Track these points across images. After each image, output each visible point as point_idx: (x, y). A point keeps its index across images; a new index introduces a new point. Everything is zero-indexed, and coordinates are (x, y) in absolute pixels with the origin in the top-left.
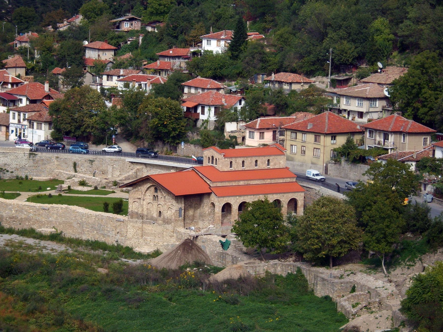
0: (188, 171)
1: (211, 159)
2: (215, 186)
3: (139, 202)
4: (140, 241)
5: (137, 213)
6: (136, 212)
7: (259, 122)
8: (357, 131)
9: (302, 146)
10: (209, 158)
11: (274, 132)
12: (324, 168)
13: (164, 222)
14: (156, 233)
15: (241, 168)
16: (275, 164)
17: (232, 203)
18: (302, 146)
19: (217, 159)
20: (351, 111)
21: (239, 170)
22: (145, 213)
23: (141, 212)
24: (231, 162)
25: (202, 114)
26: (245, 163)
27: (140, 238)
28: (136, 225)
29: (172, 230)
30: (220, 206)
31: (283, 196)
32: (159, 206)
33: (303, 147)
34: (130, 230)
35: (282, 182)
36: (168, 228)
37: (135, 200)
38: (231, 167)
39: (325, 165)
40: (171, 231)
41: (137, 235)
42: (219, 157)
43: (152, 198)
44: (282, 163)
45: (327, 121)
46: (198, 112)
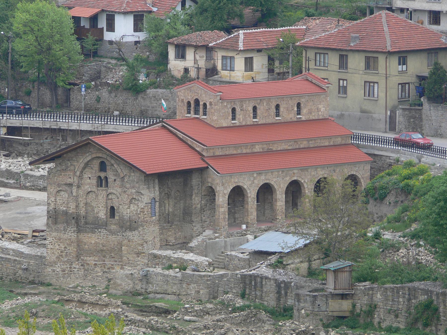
2: (212, 155)
4: (74, 265)
5: (66, 213)
6: (63, 211)
7: (242, 37)
8: (444, 46)
10: (189, 103)
11: (271, 60)
12: (388, 120)
13: (122, 227)
15: (250, 120)
16: (310, 112)
17: (245, 187)
18: (339, 80)
19: (208, 104)
20: (415, 11)
21: (249, 123)
22: (82, 212)
23: (74, 211)
24: (234, 110)
25: (108, 30)
26: (258, 112)
29: (139, 242)
30: (225, 192)
33: (341, 82)
34: (52, 247)
36: (131, 237)
37: (61, 189)
38: (234, 119)
39: (389, 113)
40: (139, 244)
41: (66, 256)
42: (212, 100)
43: (94, 182)
44: (323, 109)
45: (386, 29)
46: (100, 26)
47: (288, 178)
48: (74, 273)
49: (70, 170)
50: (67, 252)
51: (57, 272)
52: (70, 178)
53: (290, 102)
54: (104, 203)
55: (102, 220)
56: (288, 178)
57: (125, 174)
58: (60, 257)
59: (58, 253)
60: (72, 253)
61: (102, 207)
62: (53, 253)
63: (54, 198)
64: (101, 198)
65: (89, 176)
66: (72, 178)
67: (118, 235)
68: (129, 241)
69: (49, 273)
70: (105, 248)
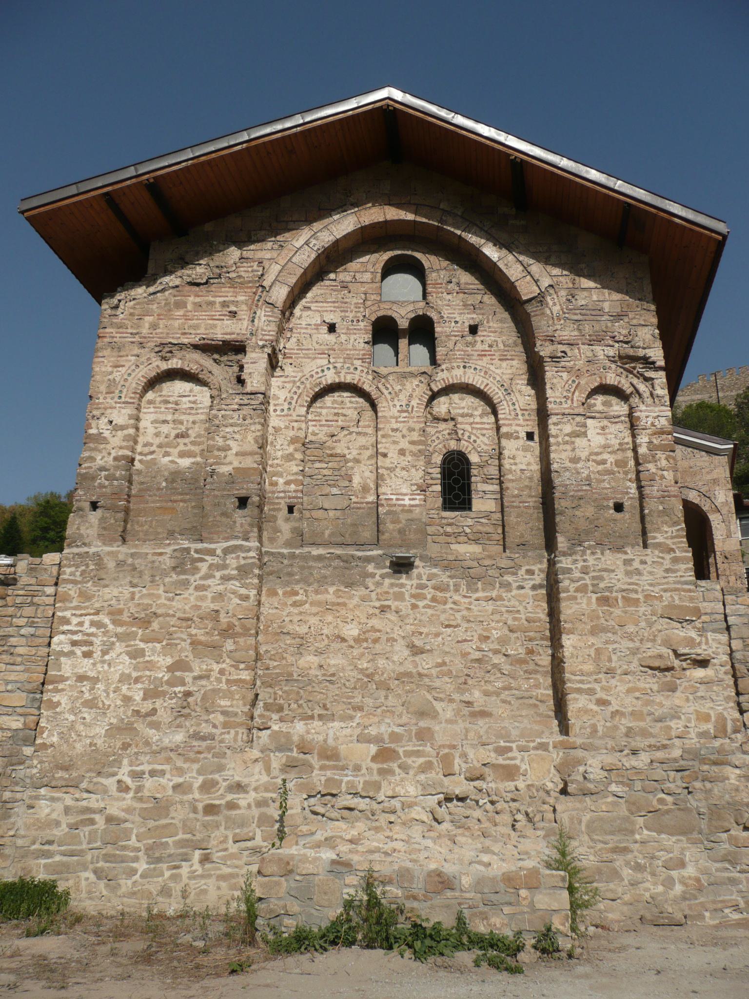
4: (234, 772)
6: (175, 476)
14: (425, 663)
27: (235, 736)
32: (442, 406)
34: (85, 666)
36: (619, 579)
41: (182, 712)
48: (231, 823)
49: (232, 283)
50: (188, 694)
51: (110, 820)
52: (233, 314)
54: (415, 436)
55: (403, 517)
57: (545, 282)
58: (140, 726)
59: (127, 699)
60: (229, 695)
61: (402, 452)
62: (91, 704)
63: (129, 411)
64: (394, 412)
65: (330, 318)
66: (244, 313)
67: (507, 586)
68: (604, 601)
69: (48, 834)
70: (425, 663)
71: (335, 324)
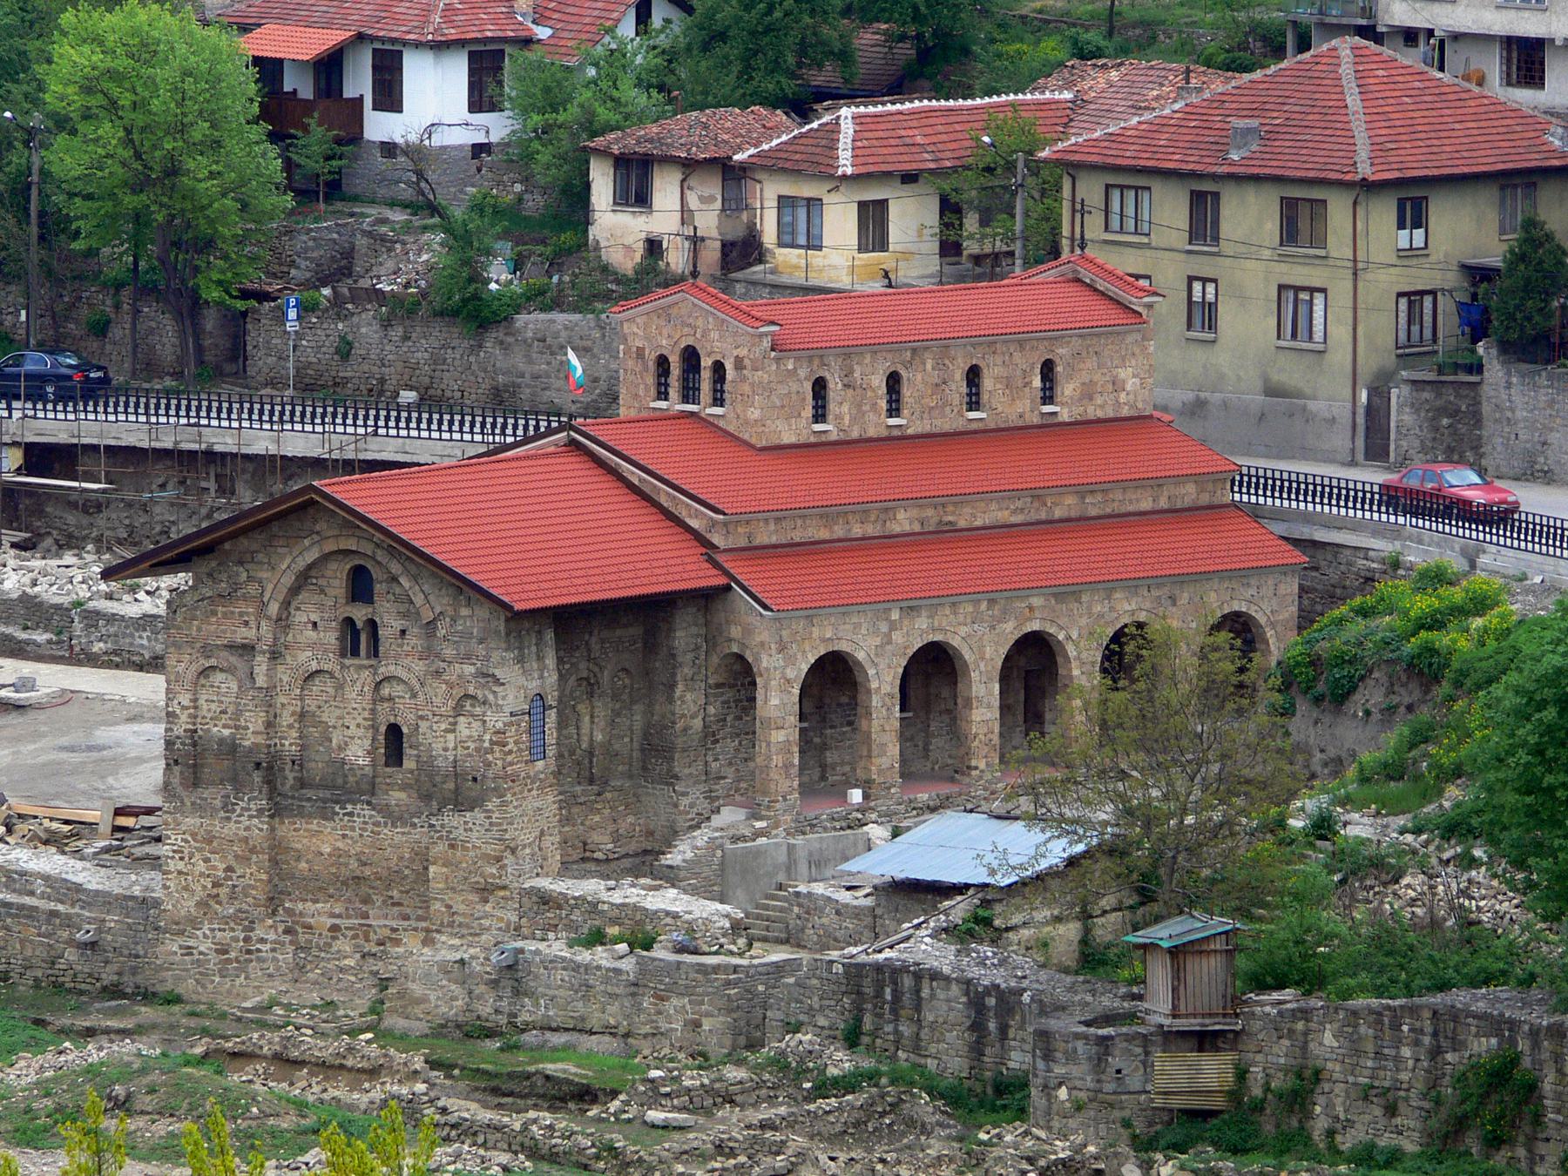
0: (536, 457)
1: (675, 371)
2: (743, 543)
3: (242, 673)
4: (259, 932)
5: (230, 748)
6: (221, 741)
7: (847, 129)
8: (1556, 163)
9: (1191, 279)
10: (662, 362)
11: (950, 209)
12: (1361, 420)
13: (426, 798)
15: (878, 423)
16: (1088, 394)
17: (860, 656)
18: (1191, 279)
19: (729, 366)
21: (872, 432)
22: (289, 744)
23: (260, 739)
24: (820, 386)
25: (377, 107)
26: (907, 392)
28: (230, 829)
30: (790, 673)
31: (1173, 600)
33: (1197, 286)
34: (181, 865)
35: (1146, 505)
36: (460, 833)
37: (213, 662)
38: (820, 415)
39: (1363, 396)
40: (486, 857)
41: (232, 897)
42: (743, 352)
43: (331, 637)
45: (1353, 100)
46: (349, 92)
47: (1009, 626)
48: (259, 960)
49: (245, 598)
50: (234, 886)
51: (201, 953)
52: (246, 623)
53: (1017, 355)
54: (366, 714)
55: (359, 773)
56: (1009, 626)
57: (438, 610)
58: (212, 903)
59: (204, 887)
60: (254, 888)
61: (358, 726)
62: (186, 888)
63: (189, 696)
64: (354, 695)
65: (314, 617)
66: (253, 624)
67: (414, 825)
68: (452, 846)
70: (367, 872)
71: (780, 197)
